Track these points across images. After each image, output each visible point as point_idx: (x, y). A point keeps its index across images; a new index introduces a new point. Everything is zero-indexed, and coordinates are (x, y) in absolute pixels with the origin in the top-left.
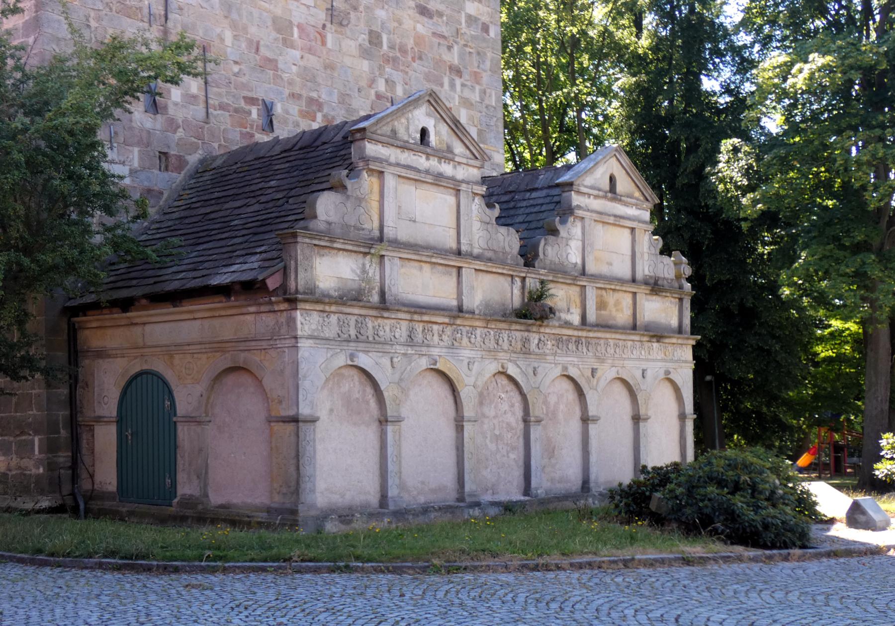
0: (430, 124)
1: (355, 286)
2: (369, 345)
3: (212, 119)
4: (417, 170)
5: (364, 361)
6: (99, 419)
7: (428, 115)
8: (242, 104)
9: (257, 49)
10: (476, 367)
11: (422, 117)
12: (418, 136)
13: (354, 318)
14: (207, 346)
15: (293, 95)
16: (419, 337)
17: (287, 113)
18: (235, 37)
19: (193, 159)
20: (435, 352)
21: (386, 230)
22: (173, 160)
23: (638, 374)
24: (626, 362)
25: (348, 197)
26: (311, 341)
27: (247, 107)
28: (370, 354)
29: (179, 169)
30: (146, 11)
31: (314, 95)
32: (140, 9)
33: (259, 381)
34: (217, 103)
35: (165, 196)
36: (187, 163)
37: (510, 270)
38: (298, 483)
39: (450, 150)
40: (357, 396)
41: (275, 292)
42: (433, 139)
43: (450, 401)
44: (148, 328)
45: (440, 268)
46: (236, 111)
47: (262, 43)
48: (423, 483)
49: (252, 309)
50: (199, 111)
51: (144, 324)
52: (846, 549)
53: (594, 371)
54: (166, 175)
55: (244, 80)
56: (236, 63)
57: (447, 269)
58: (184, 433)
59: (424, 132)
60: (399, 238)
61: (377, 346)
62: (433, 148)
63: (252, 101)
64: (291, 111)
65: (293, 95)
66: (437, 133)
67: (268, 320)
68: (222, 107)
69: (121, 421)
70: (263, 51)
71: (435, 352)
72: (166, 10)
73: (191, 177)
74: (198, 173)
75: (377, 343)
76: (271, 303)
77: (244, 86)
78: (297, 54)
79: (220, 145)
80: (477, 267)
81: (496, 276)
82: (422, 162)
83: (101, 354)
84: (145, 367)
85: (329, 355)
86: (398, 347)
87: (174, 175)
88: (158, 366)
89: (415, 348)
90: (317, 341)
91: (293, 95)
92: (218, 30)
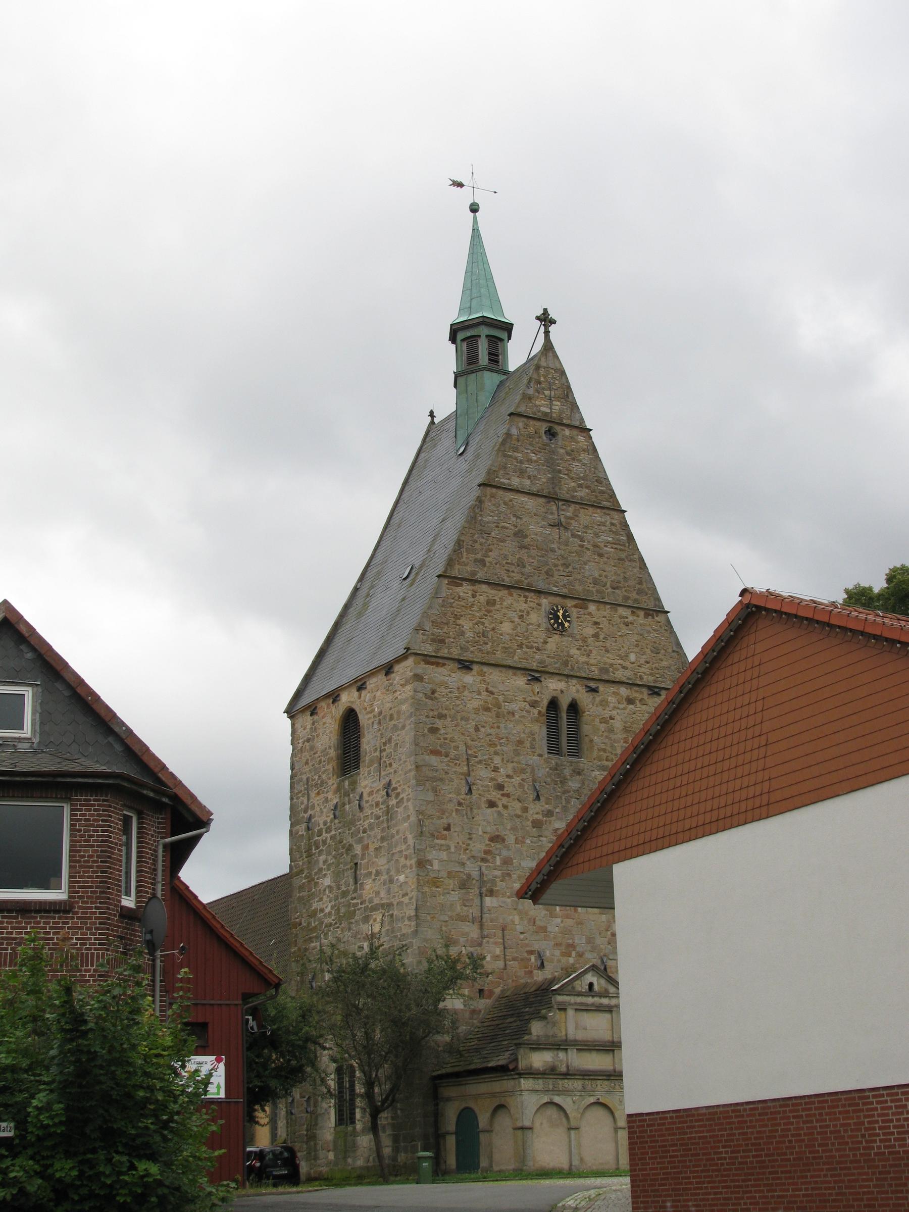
0: (594, 980)
3: (508, 967)
4: (587, 1005)
5: (557, 1099)
6: (448, 1133)
7: (593, 976)
8: (526, 955)
9: (534, 923)
11: (590, 978)
12: (587, 987)
13: (551, 1080)
15: (557, 945)
16: (589, 1088)
17: (553, 955)
18: (521, 919)
19: (498, 991)
21: (568, 1036)
22: (486, 993)
25: (548, 1023)
27: (528, 957)
29: (489, 997)
30: (471, 917)
31: (570, 941)
32: (468, 916)
33: (509, 1111)
34: (510, 958)
35: (482, 1012)
36: (494, 993)
38: (524, 1157)
39: (607, 991)
41: (513, 1070)
42: (596, 987)
43: (611, 1119)
44: (467, 1086)
46: (522, 960)
47: (537, 918)
48: (595, 1160)
49: (506, 1078)
50: (501, 964)
51: (466, 1084)
54: (483, 1001)
55: (526, 942)
56: (522, 933)
58: (483, 1138)
59: (591, 985)
60: (577, 1038)
62: (596, 992)
63: (531, 952)
64: (555, 954)
65: (557, 944)
66: (598, 984)
67: (512, 1083)
68: (514, 959)
69: (456, 1133)
70: (538, 923)
72: (481, 913)
73: (497, 1001)
74: (500, 997)
75: (566, 1092)
76: (511, 1075)
77: (527, 945)
78: (559, 920)
79: (513, 981)
82: (590, 1000)
83: (449, 1099)
84: (467, 1105)
87: (488, 1000)
88: (471, 1104)
91: (557, 945)
92: (511, 917)
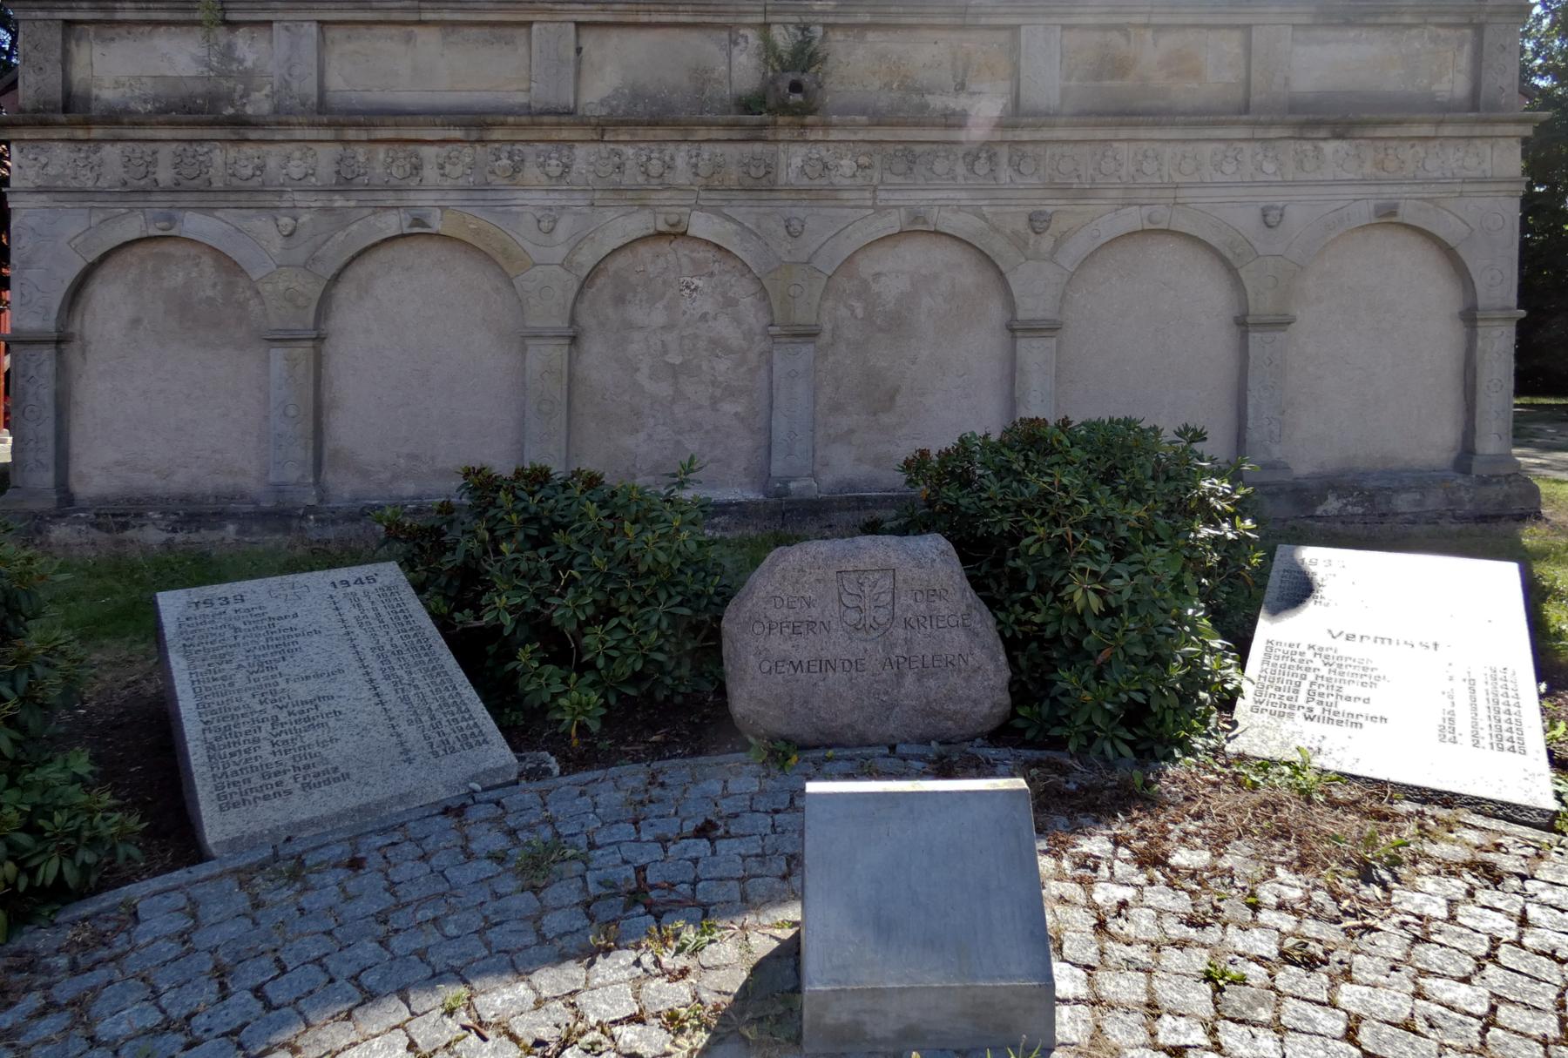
1: (199, 88)
2: (211, 196)
10: (565, 226)
14: (267, 204)
20: (425, 200)
23: (1246, 220)
24: (1181, 193)
26: (44, 197)
28: (218, 214)
37: (696, 13)
40: (210, 293)
45: (475, 31)
48: (413, 457)
52: (607, 767)
53: (1037, 222)
57: (498, 31)
61: (233, 197)
71: (425, 200)
80: (581, 18)
81: (676, 32)
85: (94, 221)
86: (297, 196)
89: (354, 195)
90: (58, 197)
